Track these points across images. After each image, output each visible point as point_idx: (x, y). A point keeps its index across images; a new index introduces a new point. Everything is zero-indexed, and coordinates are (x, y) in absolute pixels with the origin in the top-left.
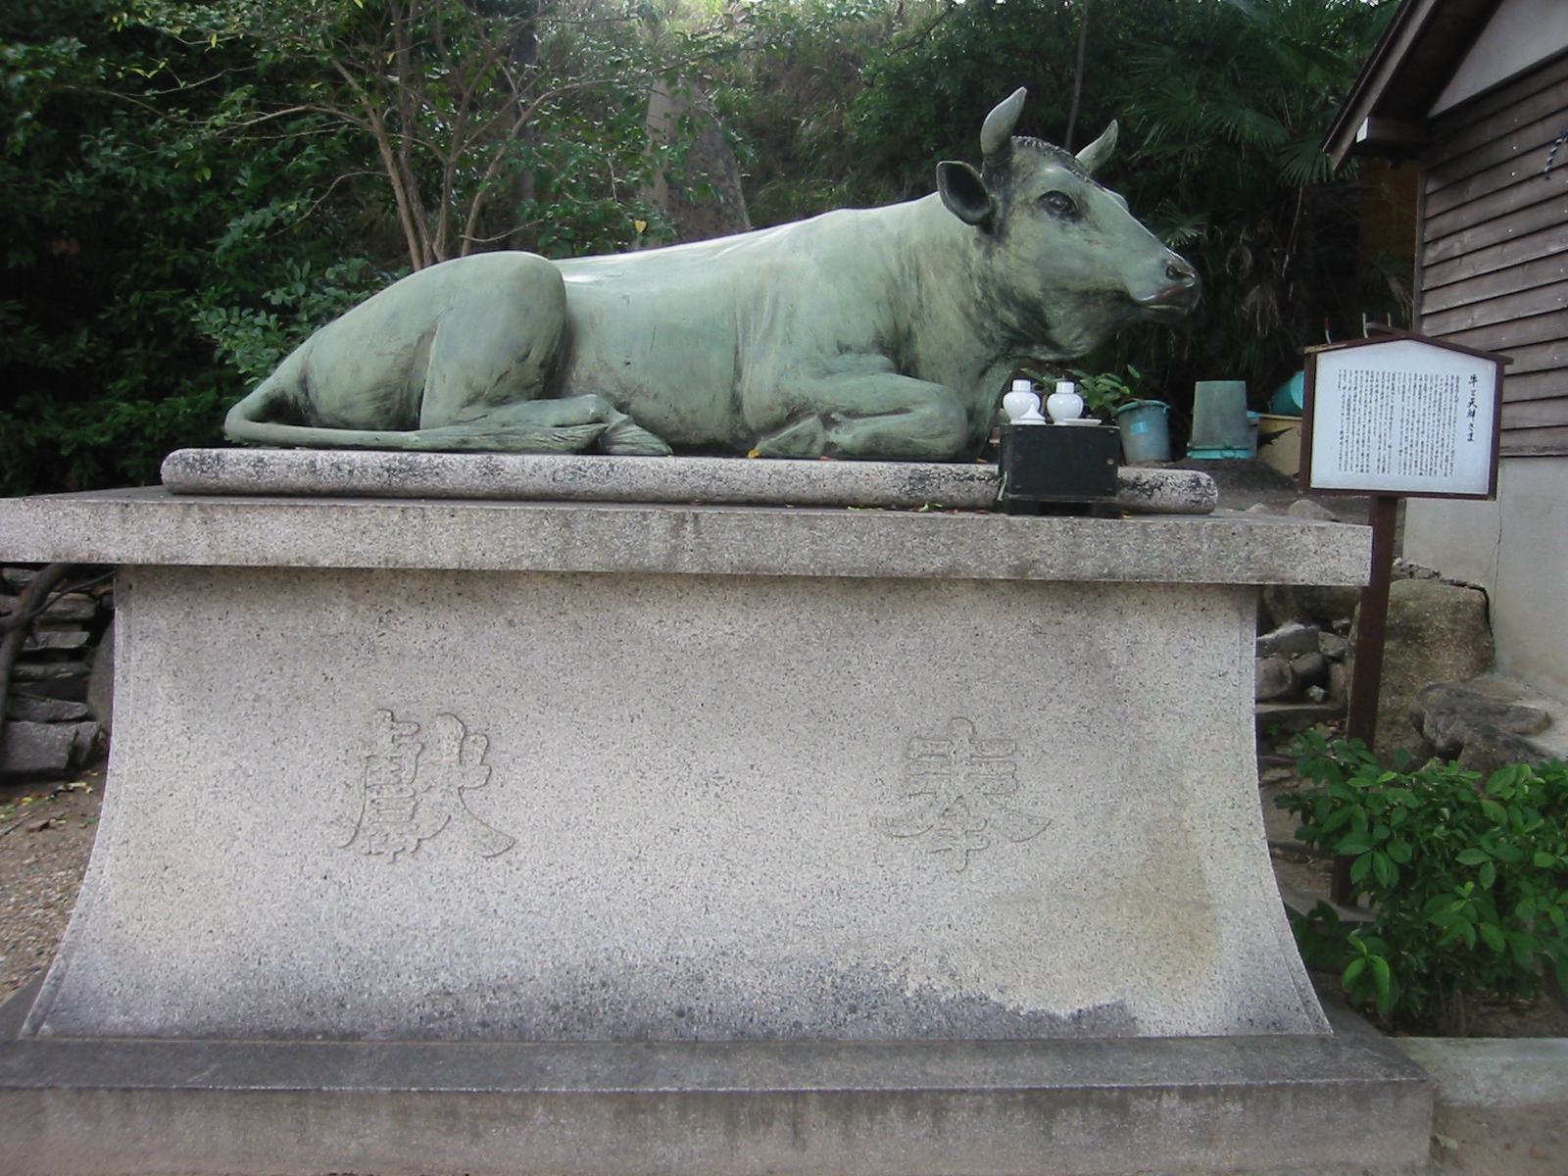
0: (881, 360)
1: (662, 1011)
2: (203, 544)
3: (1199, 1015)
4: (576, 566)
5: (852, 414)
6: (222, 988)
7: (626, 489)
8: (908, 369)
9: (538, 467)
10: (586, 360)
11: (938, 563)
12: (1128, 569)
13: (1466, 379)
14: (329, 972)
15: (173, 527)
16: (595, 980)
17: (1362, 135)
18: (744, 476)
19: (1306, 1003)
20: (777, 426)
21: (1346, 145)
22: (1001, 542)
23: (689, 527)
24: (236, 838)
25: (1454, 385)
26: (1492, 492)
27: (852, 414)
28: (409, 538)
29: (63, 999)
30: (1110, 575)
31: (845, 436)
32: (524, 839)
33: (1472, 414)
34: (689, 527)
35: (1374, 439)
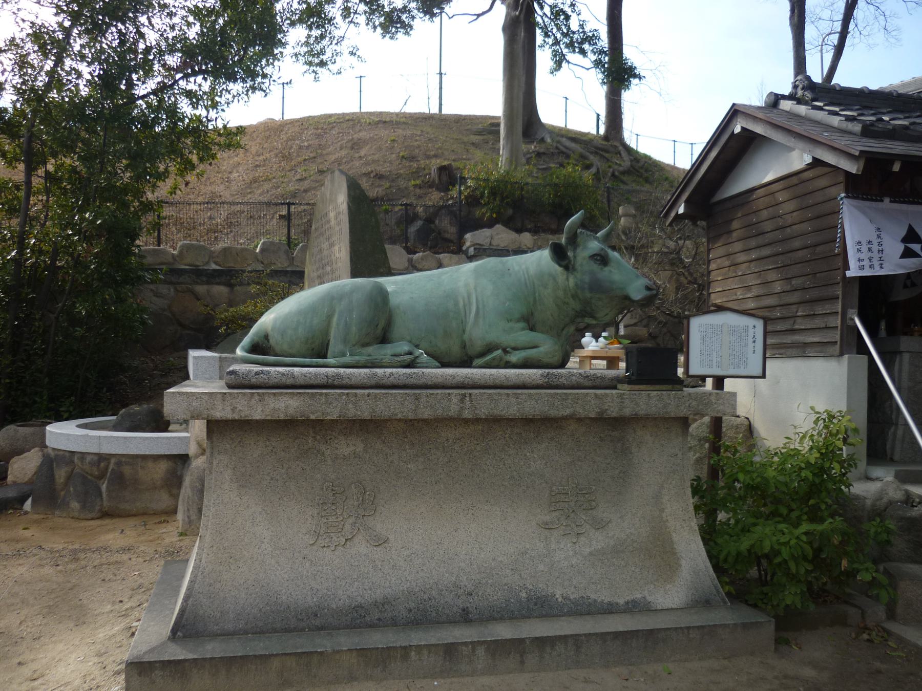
0: (522, 325)
1: (455, 609)
2: (259, 410)
3: (676, 599)
4: (420, 416)
5: (515, 349)
6: (260, 610)
7: (430, 383)
8: (532, 329)
9: (391, 374)
10: (399, 329)
11: (568, 412)
12: (642, 412)
13: (751, 327)
14: (309, 598)
15: (246, 403)
16: (426, 597)
17: (681, 210)
18: (479, 376)
19: (718, 592)
20: (482, 355)
21: (673, 214)
22: (593, 402)
23: (468, 399)
24: (263, 542)
25: (746, 329)
26: (763, 376)
27: (515, 349)
28: (350, 406)
29: (187, 620)
30: (636, 414)
31: (514, 358)
32: (391, 537)
33: (754, 342)
34: (468, 399)
35: (715, 354)
